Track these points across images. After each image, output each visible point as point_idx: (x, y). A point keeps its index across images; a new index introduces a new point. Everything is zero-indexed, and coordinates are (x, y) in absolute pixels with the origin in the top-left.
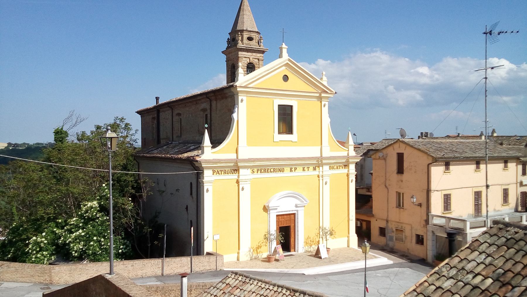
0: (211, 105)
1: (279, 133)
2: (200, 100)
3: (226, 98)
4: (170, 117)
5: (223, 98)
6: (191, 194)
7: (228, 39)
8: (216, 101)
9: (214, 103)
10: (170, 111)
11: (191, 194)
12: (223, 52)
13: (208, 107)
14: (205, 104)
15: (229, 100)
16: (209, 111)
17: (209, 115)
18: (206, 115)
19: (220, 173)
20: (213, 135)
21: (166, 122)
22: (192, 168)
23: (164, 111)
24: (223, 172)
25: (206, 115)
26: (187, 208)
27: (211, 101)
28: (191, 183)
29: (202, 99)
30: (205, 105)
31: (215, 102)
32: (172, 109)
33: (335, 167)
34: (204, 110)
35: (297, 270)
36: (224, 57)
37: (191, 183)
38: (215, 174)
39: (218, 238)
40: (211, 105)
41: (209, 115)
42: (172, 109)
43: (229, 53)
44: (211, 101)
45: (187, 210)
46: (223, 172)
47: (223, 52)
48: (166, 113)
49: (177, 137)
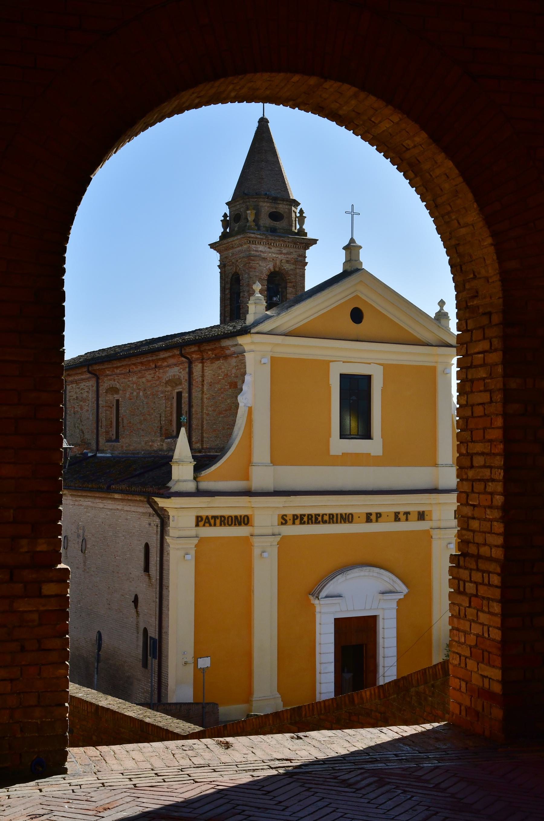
0: (190, 373)
1: (343, 436)
2: (164, 359)
3: (226, 357)
4: (92, 396)
5: (217, 358)
6: (147, 569)
7: (225, 215)
8: (202, 363)
9: (197, 368)
10: (92, 383)
11: (147, 569)
12: (213, 246)
13: (184, 375)
14: (176, 369)
15: (233, 361)
16: (185, 385)
17: (185, 395)
18: (179, 394)
19: (212, 521)
20: (194, 439)
21: (81, 408)
22: (151, 510)
23: (76, 382)
24: (218, 521)
25: (179, 394)
26: (136, 601)
27: (190, 363)
28: (147, 546)
29: (170, 357)
30: (176, 371)
31: (200, 365)
32: (98, 379)
33: (112, 398)
34: (174, 382)
35: (436, 616)
36: (215, 257)
37: (147, 546)
38: (201, 524)
39: (208, 665)
40: (190, 373)
41: (185, 395)
42: (98, 379)
43: (227, 249)
44: (190, 363)
45: (136, 606)
46: (218, 521)
47: (213, 246)
48: (82, 385)
49: (109, 440)
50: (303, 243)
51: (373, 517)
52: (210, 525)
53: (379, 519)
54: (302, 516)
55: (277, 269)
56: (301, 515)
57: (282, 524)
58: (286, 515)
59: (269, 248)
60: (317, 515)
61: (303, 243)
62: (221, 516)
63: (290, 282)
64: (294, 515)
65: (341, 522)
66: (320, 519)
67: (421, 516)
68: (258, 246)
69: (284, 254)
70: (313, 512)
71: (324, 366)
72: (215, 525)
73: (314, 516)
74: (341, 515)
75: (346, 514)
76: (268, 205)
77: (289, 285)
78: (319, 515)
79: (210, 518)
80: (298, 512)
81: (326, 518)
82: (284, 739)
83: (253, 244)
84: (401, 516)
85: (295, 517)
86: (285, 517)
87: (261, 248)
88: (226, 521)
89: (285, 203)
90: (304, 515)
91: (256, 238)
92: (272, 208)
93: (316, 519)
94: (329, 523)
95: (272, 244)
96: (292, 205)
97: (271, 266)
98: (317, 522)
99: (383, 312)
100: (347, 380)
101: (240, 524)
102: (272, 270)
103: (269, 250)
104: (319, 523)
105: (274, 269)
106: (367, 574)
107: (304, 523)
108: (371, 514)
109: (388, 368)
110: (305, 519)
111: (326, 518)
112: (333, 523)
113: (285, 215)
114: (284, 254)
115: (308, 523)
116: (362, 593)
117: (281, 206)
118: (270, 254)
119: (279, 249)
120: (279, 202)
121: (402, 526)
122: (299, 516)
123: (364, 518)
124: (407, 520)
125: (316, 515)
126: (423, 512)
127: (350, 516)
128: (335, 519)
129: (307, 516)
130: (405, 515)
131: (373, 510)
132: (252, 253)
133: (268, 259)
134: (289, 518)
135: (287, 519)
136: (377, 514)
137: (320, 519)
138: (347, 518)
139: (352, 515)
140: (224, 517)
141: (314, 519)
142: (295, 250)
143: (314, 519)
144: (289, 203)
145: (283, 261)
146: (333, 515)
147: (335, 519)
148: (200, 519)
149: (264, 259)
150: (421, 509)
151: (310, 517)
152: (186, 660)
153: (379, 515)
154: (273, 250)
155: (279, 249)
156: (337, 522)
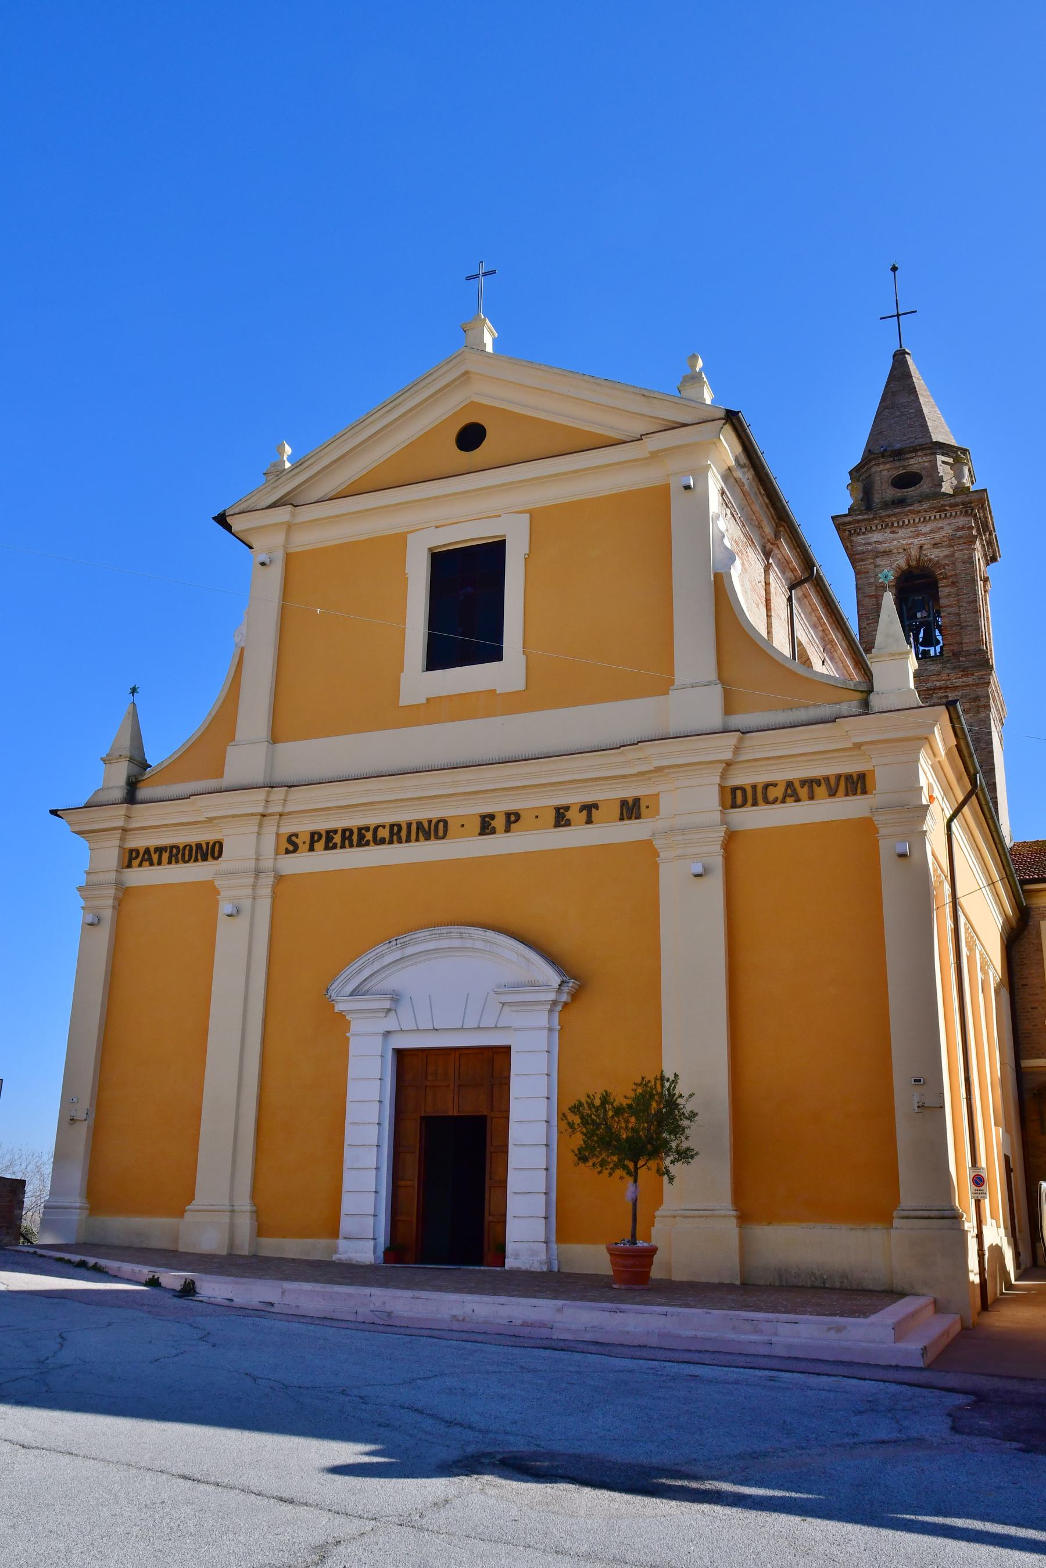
19: (155, 857)
24: (165, 856)
46: (165, 856)
50: (956, 505)
51: (499, 823)
52: (152, 864)
53: (513, 826)
54: (330, 834)
55: (913, 563)
56: (328, 832)
57: (287, 852)
58: (296, 835)
59: (893, 532)
60: (363, 830)
61: (956, 505)
62: (172, 847)
63: (944, 578)
64: (313, 834)
65: (417, 840)
66: (369, 836)
67: (631, 810)
68: (870, 535)
69: (925, 534)
70: (353, 822)
71: (396, 545)
72: (159, 863)
73: (356, 832)
74: (419, 824)
75: (430, 822)
76: (888, 466)
77: (941, 583)
78: (367, 829)
79: (152, 850)
80: (322, 825)
81: (383, 833)
82: (239, 1301)
83: (859, 534)
84: (572, 814)
85: (314, 837)
86: (294, 838)
87: (876, 537)
88: (180, 856)
89: (920, 453)
90: (335, 832)
91: (859, 521)
92: (898, 468)
93: (361, 837)
94: (391, 842)
95: (896, 524)
96: (935, 454)
97: (902, 562)
98: (362, 842)
99: (535, 415)
100: (444, 563)
101: (205, 859)
102: (904, 566)
103: (892, 536)
104: (367, 844)
105: (908, 564)
106: (457, 943)
107: (334, 847)
108: (492, 817)
109: (540, 520)
110: (337, 839)
111: (383, 833)
112: (400, 841)
113: (924, 473)
114: (925, 534)
115: (343, 847)
116: (464, 990)
117: (912, 461)
118: (895, 542)
119: (913, 529)
120: (908, 456)
121: (578, 836)
122: (324, 834)
123: (477, 824)
124: (589, 821)
125: (360, 829)
126: (637, 801)
127: (441, 825)
128: (404, 834)
129: (340, 832)
130: (585, 812)
131: (499, 806)
132: (859, 548)
133: (895, 551)
134: (303, 840)
135: (298, 841)
136: (508, 815)
137: (369, 836)
138: (432, 830)
139: (445, 822)
140: (177, 847)
141: (355, 838)
142: (947, 521)
143: (355, 838)
144: (929, 452)
145: (925, 547)
146: (399, 826)
147: (404, 834)
148: (134, 855)
149: (887, 553)
150: (629, 793)
151: (347, 834)
152: (73, 1113)
153: (512, 819)
154: (901, 533)
155: (913, 529)
156: (408, 840)
